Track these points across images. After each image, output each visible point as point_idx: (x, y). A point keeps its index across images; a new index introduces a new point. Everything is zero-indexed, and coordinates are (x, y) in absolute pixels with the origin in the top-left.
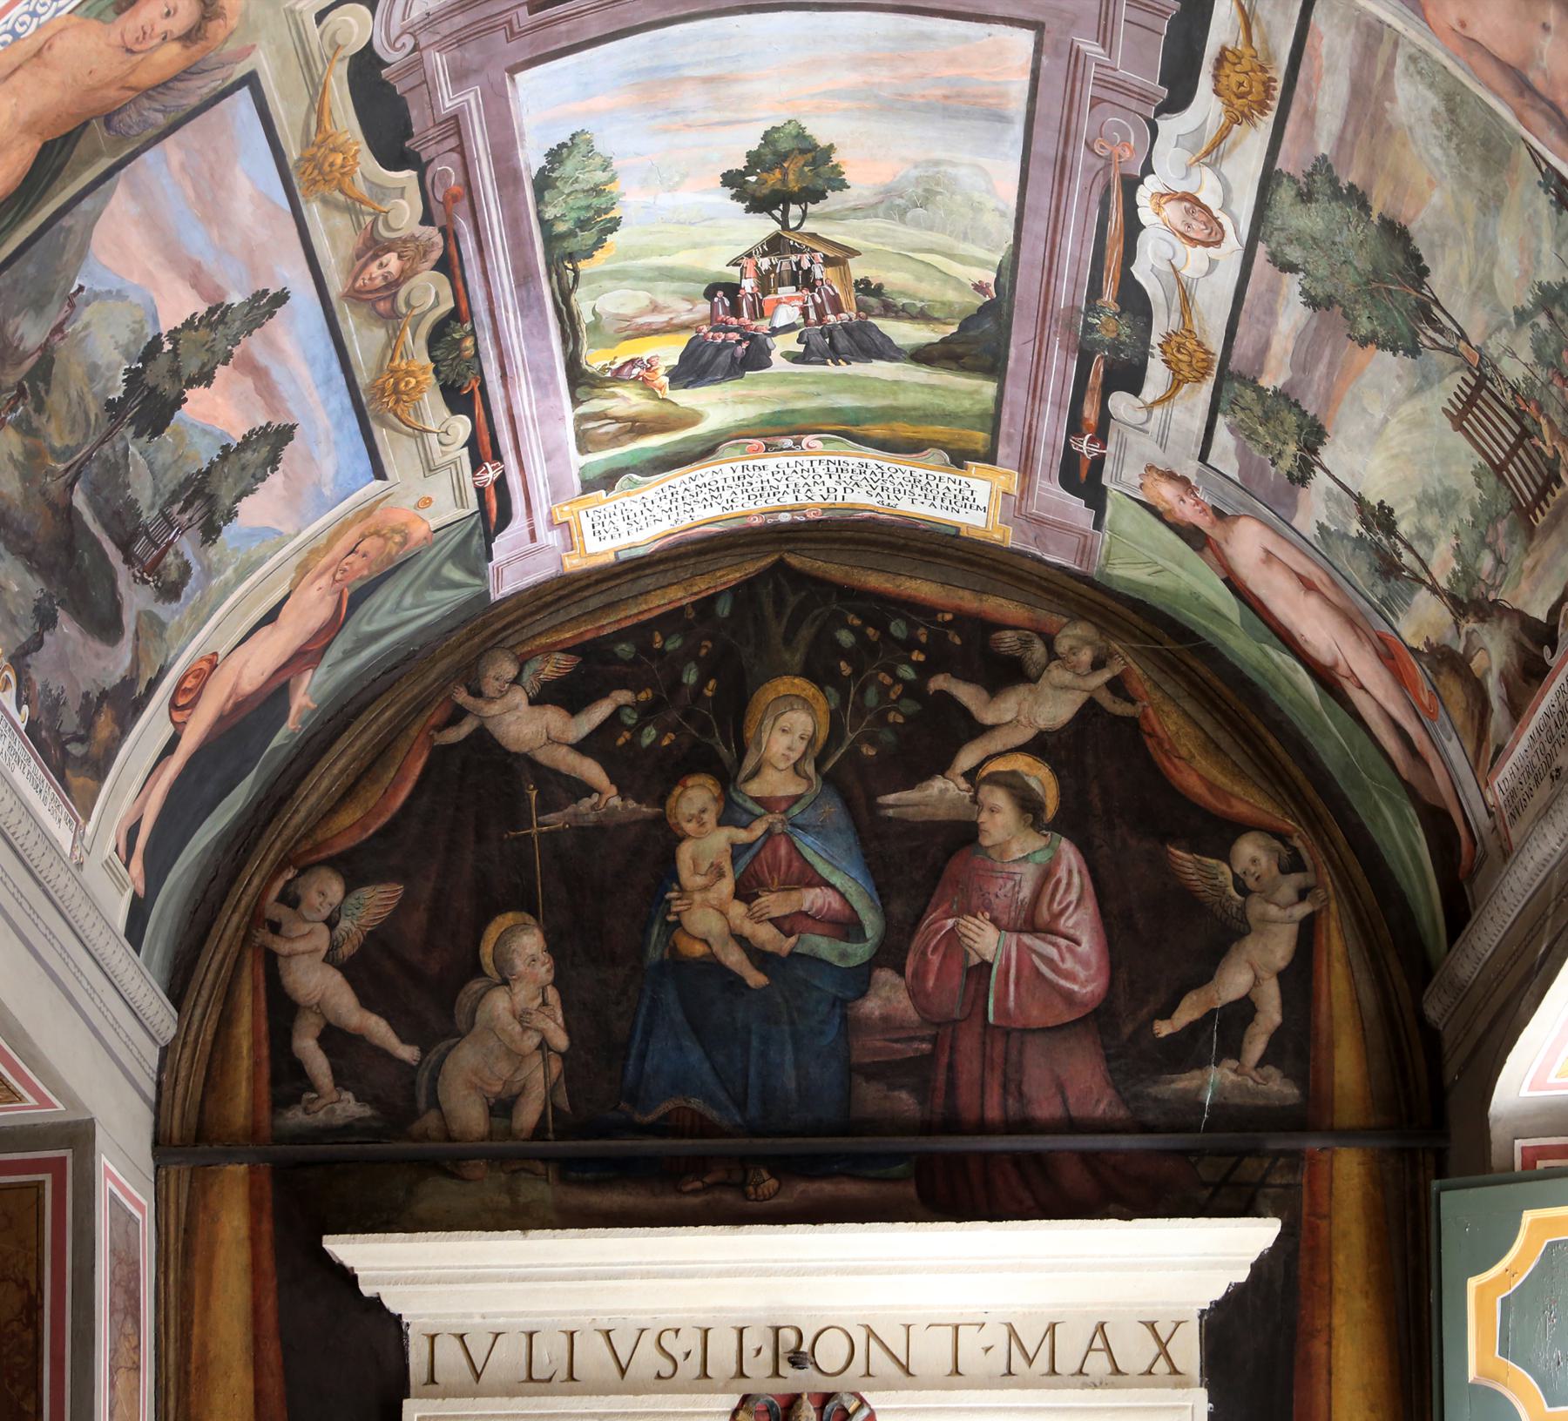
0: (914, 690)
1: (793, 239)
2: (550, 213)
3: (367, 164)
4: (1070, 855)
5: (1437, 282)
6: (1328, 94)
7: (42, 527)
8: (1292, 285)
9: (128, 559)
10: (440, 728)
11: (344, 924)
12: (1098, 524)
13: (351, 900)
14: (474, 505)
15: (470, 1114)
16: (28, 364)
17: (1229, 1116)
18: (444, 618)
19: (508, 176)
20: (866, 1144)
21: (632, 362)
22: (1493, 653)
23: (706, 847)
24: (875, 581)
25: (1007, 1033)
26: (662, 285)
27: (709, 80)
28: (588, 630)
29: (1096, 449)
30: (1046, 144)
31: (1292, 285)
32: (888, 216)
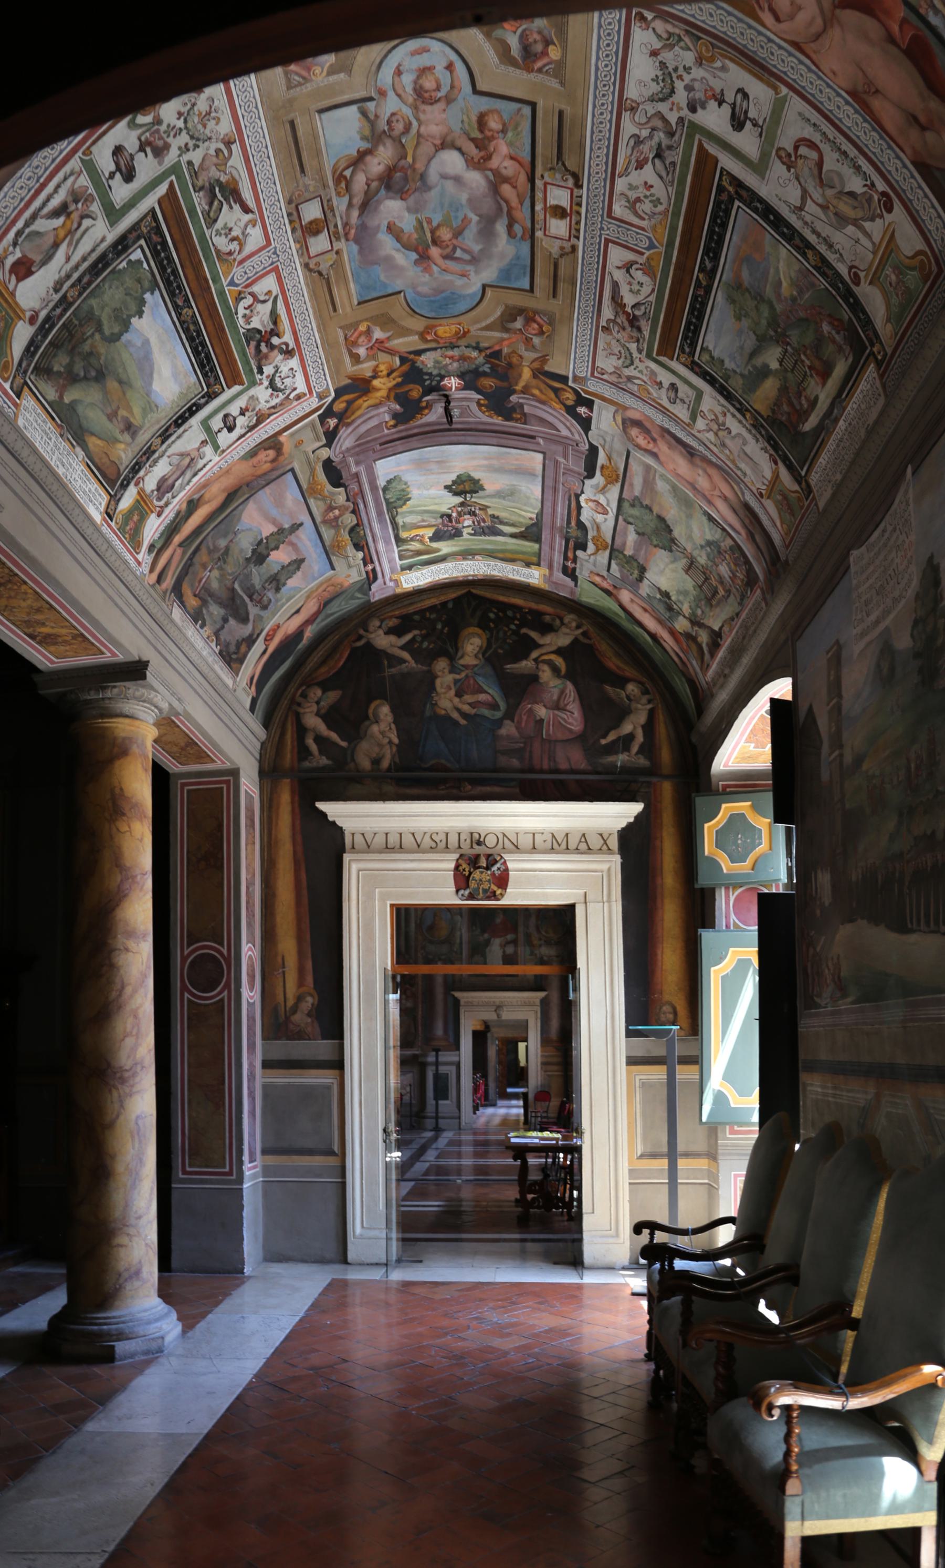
0: (516, 633)
3: (329, 487)
4: (570, 687)
5: (676, 533)
7: (224, 595)
8: (631, 528)
12: (576, 585)
14: (364, 575)
15: (366, 764)
17: (625, 770)
19: (374, 487)
20: (502, 775)
22: (704, 638)
23: (445, 679)
24: (501, 598)
25: (550, 741)
28: (404, 611)
30: (549, 482)
31: (631, 528)
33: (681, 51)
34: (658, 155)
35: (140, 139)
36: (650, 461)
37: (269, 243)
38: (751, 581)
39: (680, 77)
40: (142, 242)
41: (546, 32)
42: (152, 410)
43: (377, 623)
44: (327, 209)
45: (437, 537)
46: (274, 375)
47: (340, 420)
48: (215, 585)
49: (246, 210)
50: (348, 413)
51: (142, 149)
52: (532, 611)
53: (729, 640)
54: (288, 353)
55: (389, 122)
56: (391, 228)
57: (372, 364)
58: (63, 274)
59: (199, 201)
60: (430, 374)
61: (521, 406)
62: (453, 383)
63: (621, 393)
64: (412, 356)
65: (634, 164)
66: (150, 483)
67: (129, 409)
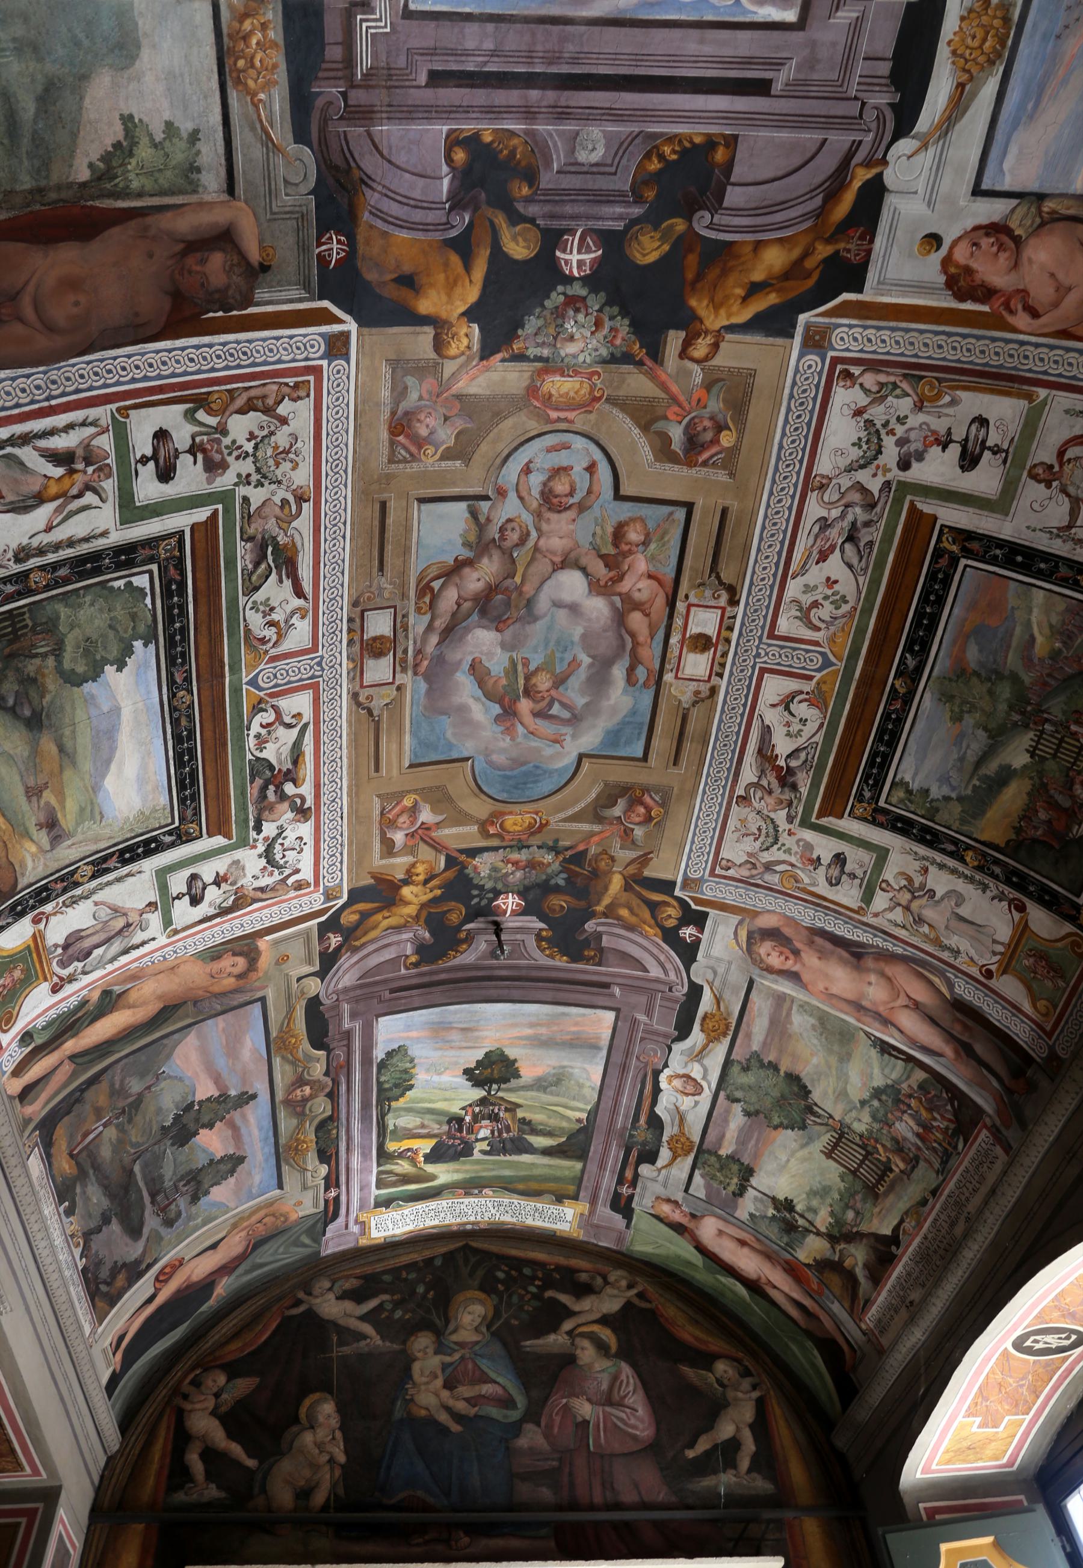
1: (492, 1100)
2: (383, 1079)
3: (306, 1045)
4: (626, 1370)
5: (816, 1096)
6: (758, 1027)
9: (153, 1203)
10: (288, 1308)
11: (225, 1396)
12: (628, 1226)
13: (230, 1385)
16: (131, 1100)
17: (734, 1500)
18: (296, 1261)
19: (367, 1060)
21: (409, 1150)
22: (857, 1256)
23: (427, 1361)
24: (514, 1252)
25: (602, 1456)
26: (428, 1116)
27: (463, 1029)
28: (368, 1270)
29: (630, 1191)
30: (617, 1058)
31: (737, 1108)
32: (538, 1090)
33: (895, 400)
34: (851, 538)
35: (193, 440)
36: (785, 987)
37: (315, 648)
38: (966, 1119)
39: (892, 432)
40: (154, 567)
41: (720, 417)
42: (92, 818)
43: (327, 1284)
44: (400, 625)
45: (434, 1157)
46: (274, 839)
47: (346, 940)
48: (106, 1153)
49: (299, 593)
50: (358, 933)
51: (192, 451)
52: (558, 1268)
53: (917, 1240)
54: (302, 813)
55: (502, 530)
56: (477, 669)
57: (407, 859)
58: (35, 542)
59: (244, 553)
60: (481, 888)
61: (598, 936)
62: (510, 902)
63: (752, 892)
64: (463, 858)
65: (815, 555)
66: (57, 931)
67: (61, 796)
